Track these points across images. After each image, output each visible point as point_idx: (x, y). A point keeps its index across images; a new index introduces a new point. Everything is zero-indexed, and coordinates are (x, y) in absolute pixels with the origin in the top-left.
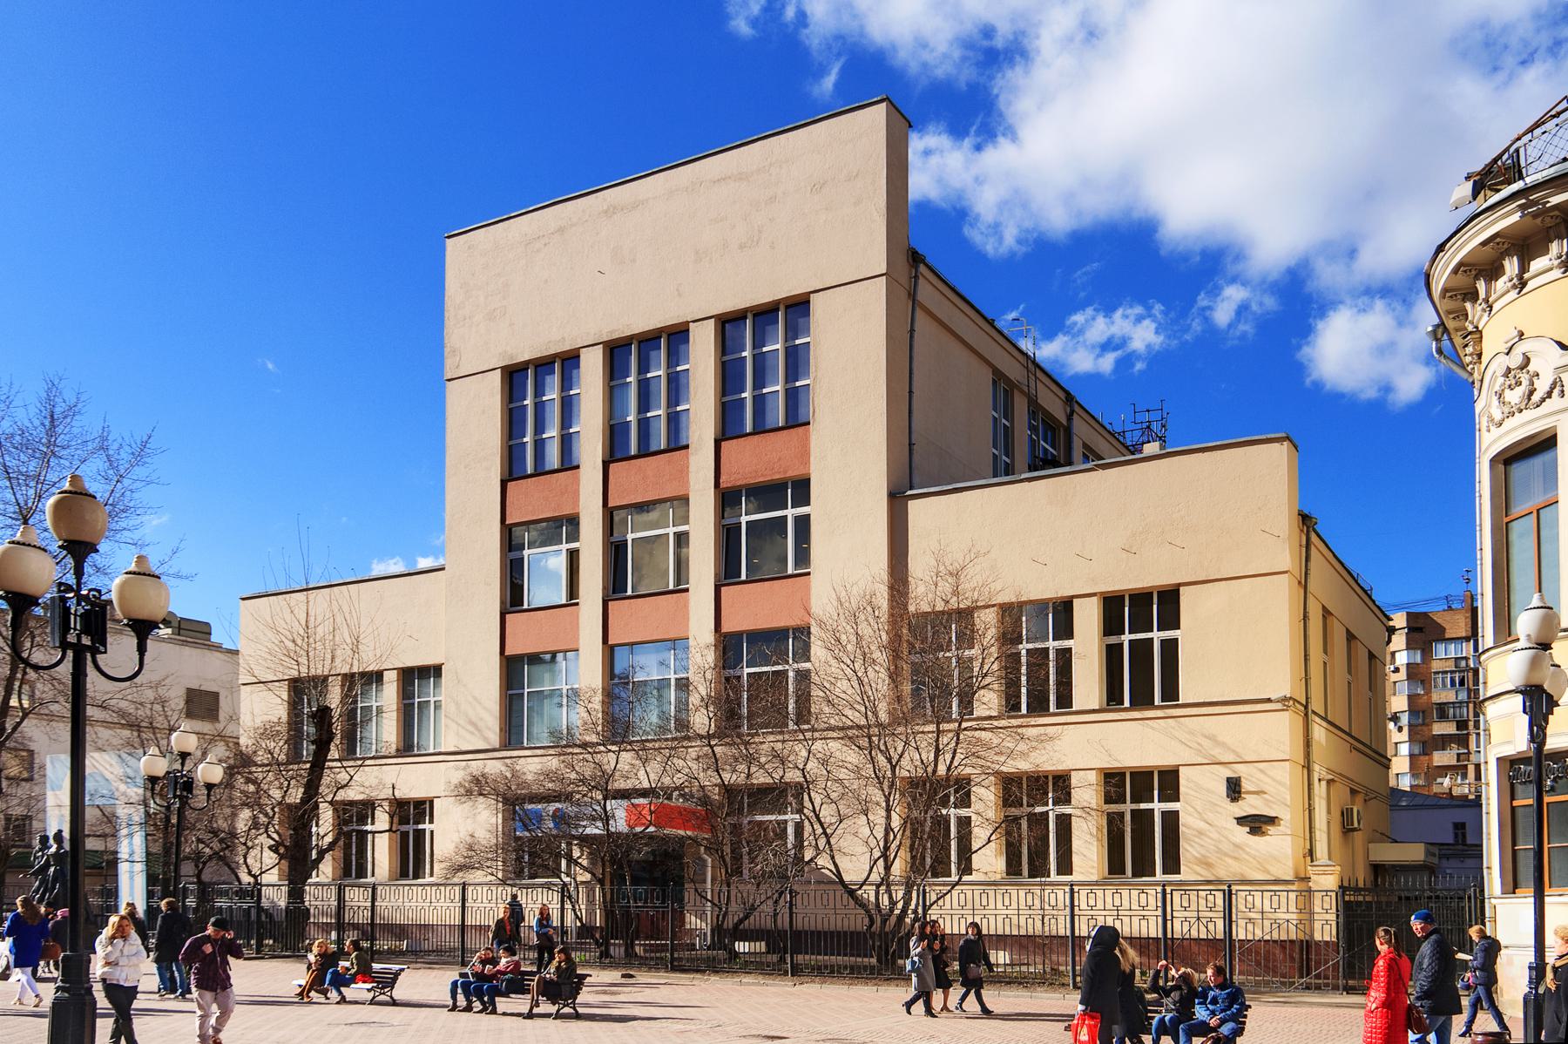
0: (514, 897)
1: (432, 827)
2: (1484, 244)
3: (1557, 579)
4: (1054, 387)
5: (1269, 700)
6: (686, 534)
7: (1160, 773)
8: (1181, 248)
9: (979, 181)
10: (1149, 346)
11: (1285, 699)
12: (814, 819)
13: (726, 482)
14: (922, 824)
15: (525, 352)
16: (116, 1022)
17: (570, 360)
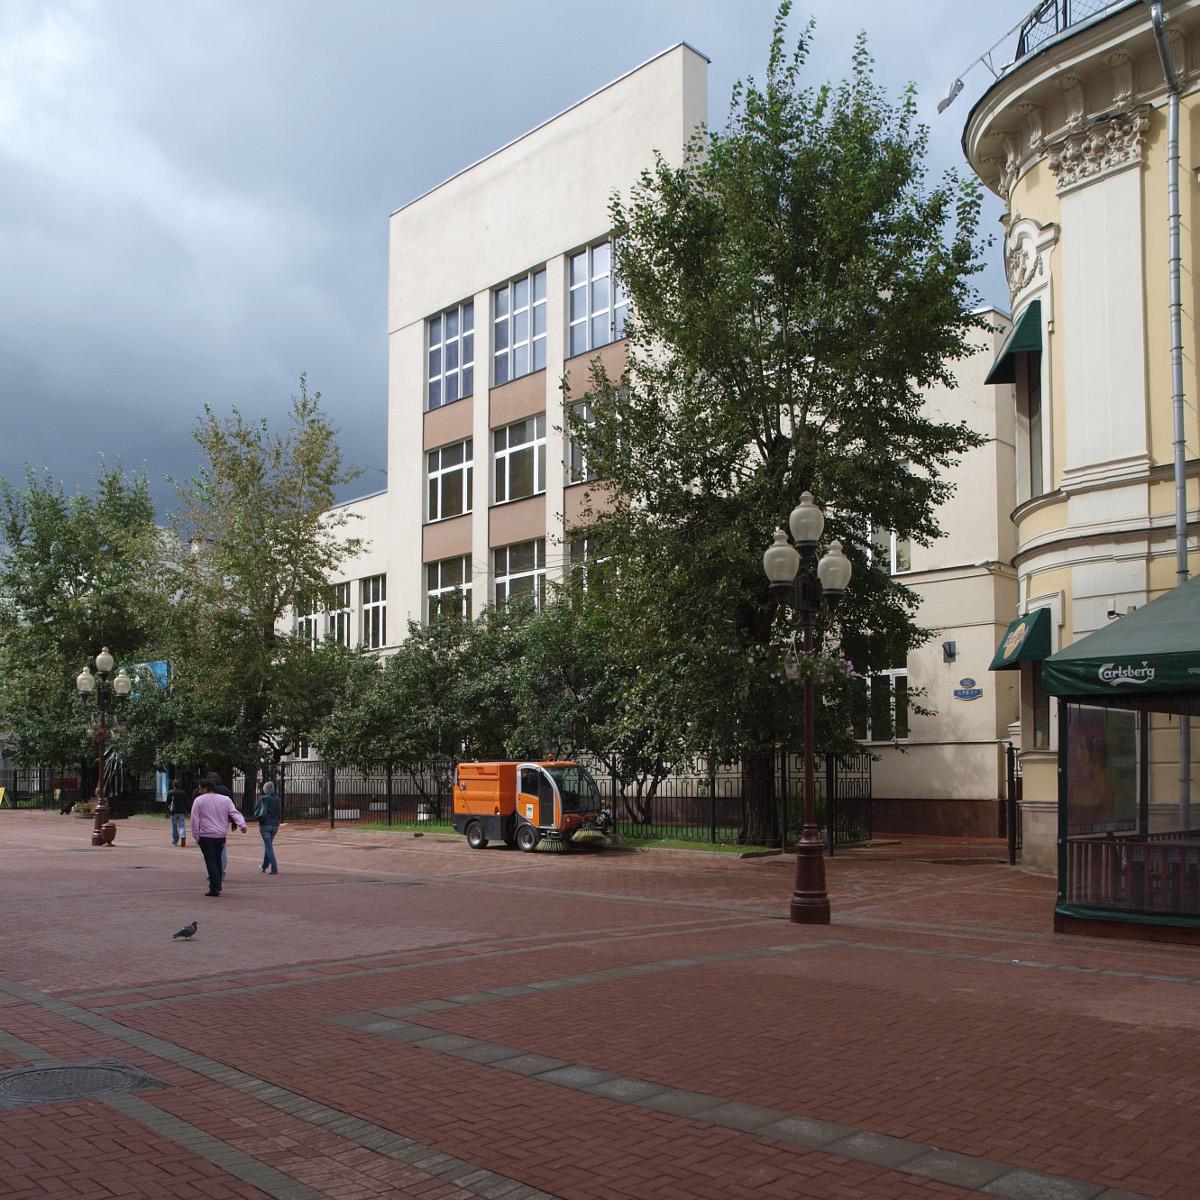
0: (974, 440)
1: (470, 464)
2: (1010, 106)
3: (500, 283)
4: (960, 574)
5: (972, 566)
6: (471, 337)
7: (533, 566)
8: (371, 825)
9: (912, 616)
10: (1151, 148)
11: (986, 565)
12: (290, 969)
13: (491, 546)
14: (167, 580)
15: (366, 575)
16: (1023, 738)
17: (468, 304)
